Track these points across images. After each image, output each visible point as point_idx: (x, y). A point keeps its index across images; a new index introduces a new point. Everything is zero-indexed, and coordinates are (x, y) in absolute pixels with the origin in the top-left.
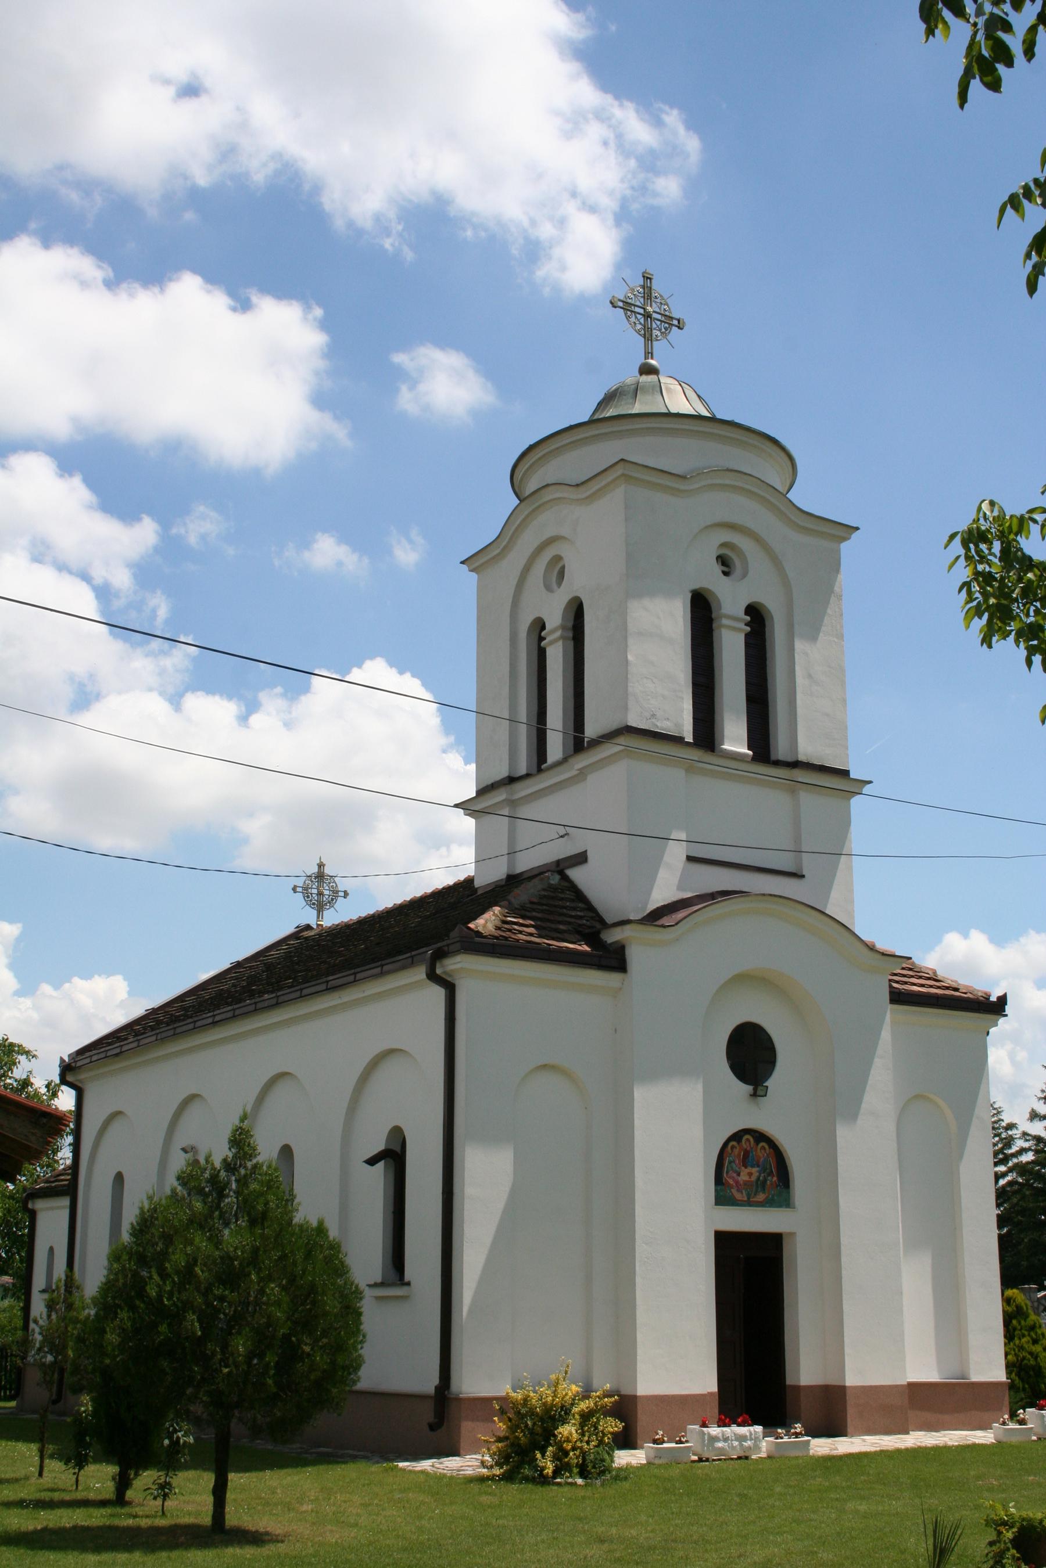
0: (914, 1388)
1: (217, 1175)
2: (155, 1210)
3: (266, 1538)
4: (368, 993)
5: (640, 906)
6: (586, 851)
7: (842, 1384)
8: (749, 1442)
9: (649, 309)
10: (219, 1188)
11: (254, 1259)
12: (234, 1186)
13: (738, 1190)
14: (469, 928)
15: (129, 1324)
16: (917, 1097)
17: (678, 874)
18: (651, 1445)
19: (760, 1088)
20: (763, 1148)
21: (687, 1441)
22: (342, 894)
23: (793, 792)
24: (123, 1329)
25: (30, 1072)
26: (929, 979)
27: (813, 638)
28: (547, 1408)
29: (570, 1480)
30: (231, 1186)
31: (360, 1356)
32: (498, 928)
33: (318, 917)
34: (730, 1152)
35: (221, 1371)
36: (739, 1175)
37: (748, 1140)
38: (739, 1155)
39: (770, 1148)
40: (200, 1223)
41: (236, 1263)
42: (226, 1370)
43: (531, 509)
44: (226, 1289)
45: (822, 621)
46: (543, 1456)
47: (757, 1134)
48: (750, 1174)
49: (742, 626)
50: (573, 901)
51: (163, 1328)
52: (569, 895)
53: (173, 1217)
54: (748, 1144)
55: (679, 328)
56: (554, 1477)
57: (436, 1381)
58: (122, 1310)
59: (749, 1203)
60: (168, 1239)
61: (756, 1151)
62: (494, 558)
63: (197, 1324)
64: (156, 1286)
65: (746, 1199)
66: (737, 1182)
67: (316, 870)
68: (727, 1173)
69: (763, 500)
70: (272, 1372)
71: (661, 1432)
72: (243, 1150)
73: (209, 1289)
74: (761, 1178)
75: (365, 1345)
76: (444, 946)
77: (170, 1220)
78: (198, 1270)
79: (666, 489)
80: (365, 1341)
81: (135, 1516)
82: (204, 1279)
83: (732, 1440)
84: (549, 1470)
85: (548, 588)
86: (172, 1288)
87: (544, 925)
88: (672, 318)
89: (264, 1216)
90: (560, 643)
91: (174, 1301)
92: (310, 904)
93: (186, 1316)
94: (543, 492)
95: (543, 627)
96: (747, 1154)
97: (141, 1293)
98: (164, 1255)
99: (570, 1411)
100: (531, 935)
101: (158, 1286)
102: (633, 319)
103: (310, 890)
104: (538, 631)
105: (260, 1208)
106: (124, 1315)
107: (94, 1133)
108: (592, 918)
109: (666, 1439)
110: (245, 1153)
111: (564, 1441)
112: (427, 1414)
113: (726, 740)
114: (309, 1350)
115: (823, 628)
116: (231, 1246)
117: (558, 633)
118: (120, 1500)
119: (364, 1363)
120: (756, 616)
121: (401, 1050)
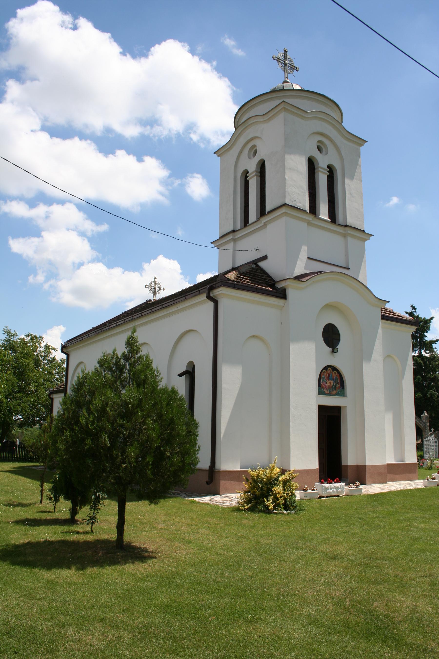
0: (389, 466)
1: (119, 361)
2: (86, 378)
3: (146, 554)
4: (179, 308)
6: (267, 255)
8: (340, 490)
9: (286, 62)
10: (120, 368)
11: (140, 404)
12: (128, 367)
14: (225, 277)
15: (70, 440)
16: (388, 356)
17: (305, 263)
18: (302, 491)
19: (335, 349)
20: (335, 373)
21: (316, 490)
22: (162, 289)
23: (345, 236)
24: (67, 441)
25: (56, 355)
26: (391, 312)
27: (352, 178)
28: (269, 479)
29: (281, 512)
30: (127, 367)
31: (197, 458)
32: (236, 278)
33: (154, 297)
35: (121, 466)
36: (326, 383)
37: (330, 370)
38: (327, 375)
40: (112, 385)
41: (130, 406)
42: (124, 466)
43: (243, 128)
44: (124, 420)
45: (355, 174)
46: (267, 500)
47: (333, 368)
48: (330, 383)
49: (326, 172)
50: (261, 273)
51: (88, 441)
52: (259, 271)
53: (95, 381)
55: (297, 70)
56: (273, 510)
57: (209, 464)
58: (66, 430)
59: (330, 394)
60: (92, 393)
61: (332, 374)
62: (227, 149)
63: (107, 440)
64: (85, 418)
66: (326, 386)
67: (153, 280)
68: (322, 382)
69: (334, 126)
70: (150, 467)
71: (306, 486)
72: (133, 348)
73: (115, 420)
75: (199, 452)
76: (214, 285)
77: (93, 383)
78: (108, 409)
80: (199, 450)
81: (78, 533)
82: (112, 415)
84: (271, 507)
85: (250, 158)
86: (94, 419)
87: (254, 280)
88: (294, 66)
89: (145, 382)
90: (255, 177)
91: (95, 426)
93: (101, 435)
94: (249, 120)
95: (248, 172)
96: (329, 375)
97: (77, 422)
98: (90, 402)
99: (278, 480)
100: (249, 282)
101: (87, 418)
102: (280, 65)
104: (246, 173)
105: (142, 377)
106: (68, 433)
107: (74, 368)
108: (270, 280)
109: (308, 489)
110: (134, 350)
111: (277, 494)
112: (206, 478)
113: (321, 214)
114: (169, 455)
115: (355, 177)
116: (127, 397)
117: (254, 174)
118: (72, 521)
119: (199, 462)
120: (331, 171)
121: (193, 330)
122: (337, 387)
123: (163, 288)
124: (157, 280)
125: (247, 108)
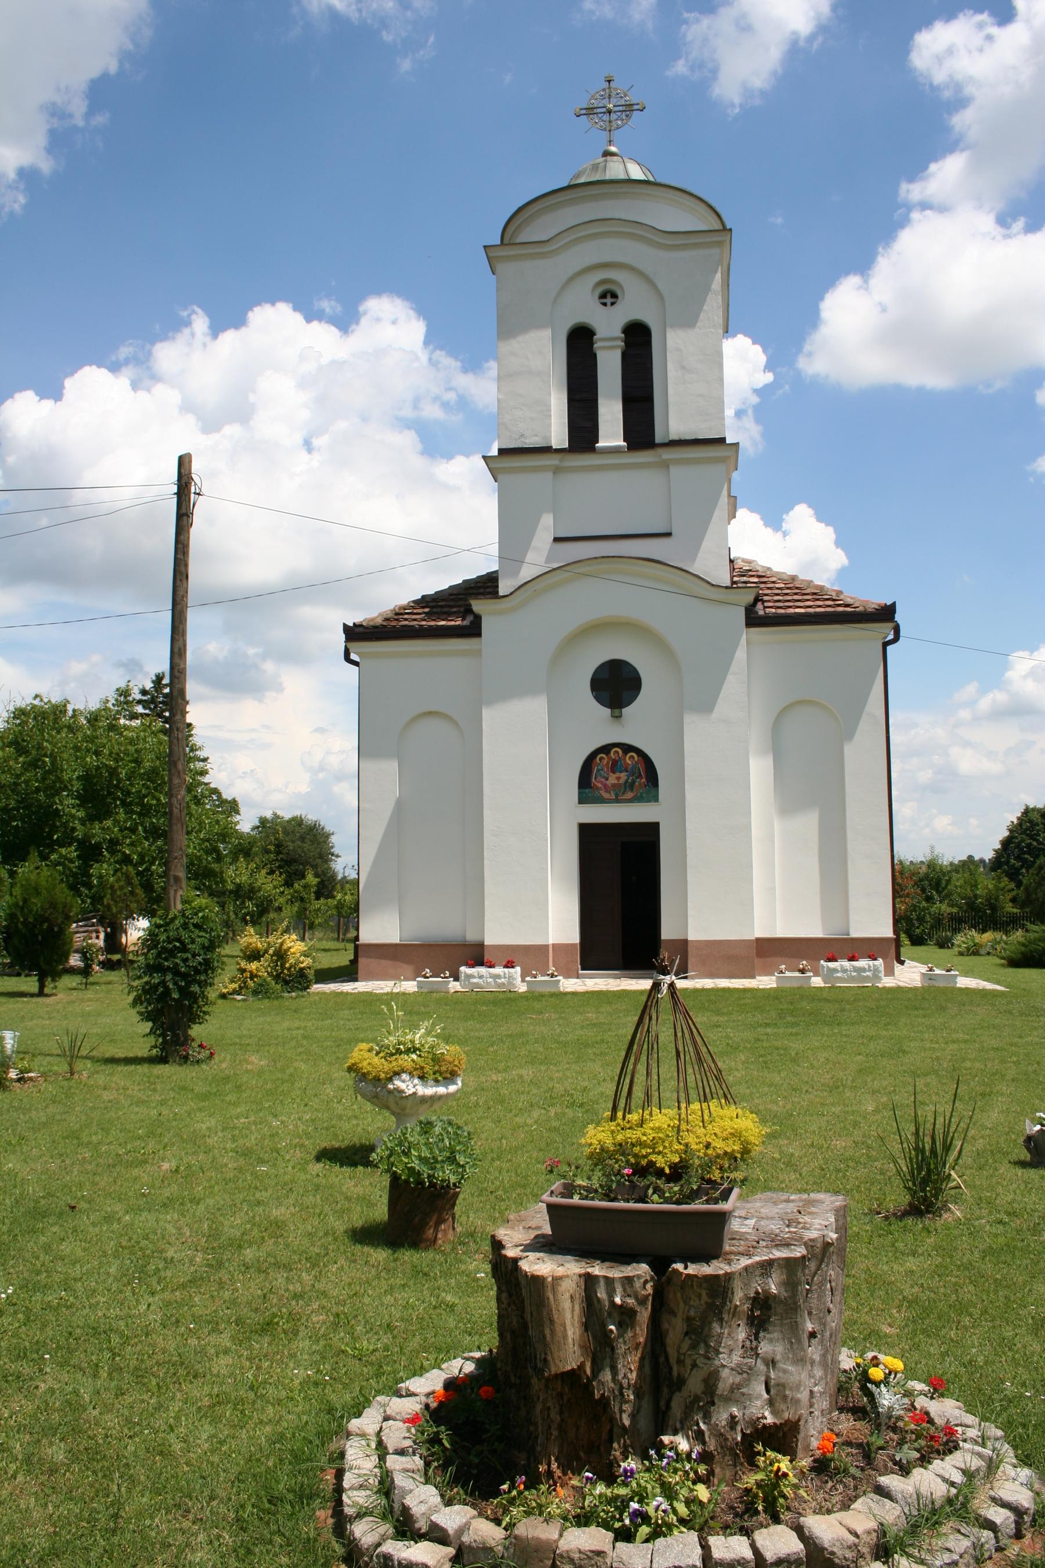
7: (471, 937)
36: (607, 779)
37: (616, 752)
38: (608, 763)
48: (618, 778)
59: (617, 800)
66: (605, 786)
79: (542, 255)
115: (698, 324)
125: (596, 231)
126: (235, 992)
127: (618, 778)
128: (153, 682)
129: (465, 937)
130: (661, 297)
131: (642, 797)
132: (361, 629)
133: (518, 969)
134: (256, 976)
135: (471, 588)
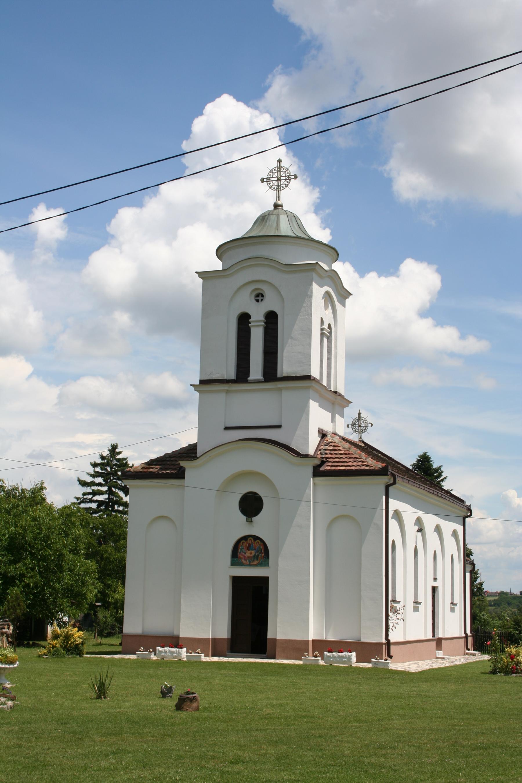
5: (202, 451)
7: (175, 633)
13: (245, 560)
34: (242, 544)
36: (245, 553)
37: (251, 539)
38: (246, 545)
39: (261, 542)
48: (251, 553)
54: (250, 541)
59: (250, 565)
65: (248, 563)
66: (244, 557)
67: (357, 416)
68: (240, 553)
74: (256, 555)
83: (168, 653)
92: (355, 431)
96: (249, 545)
103: (355, 426)
122: (260, 556)
123: (348, 427)
124: (362, 415)
126: (45, 654)
127: (251, 553)
128: (109, 450)
129: (173, 633)
130: (283, 299)
131: (262, 563)
132: (130, 473)
133: (185, 650)
134: (55, 647)
135: (191, 449)
